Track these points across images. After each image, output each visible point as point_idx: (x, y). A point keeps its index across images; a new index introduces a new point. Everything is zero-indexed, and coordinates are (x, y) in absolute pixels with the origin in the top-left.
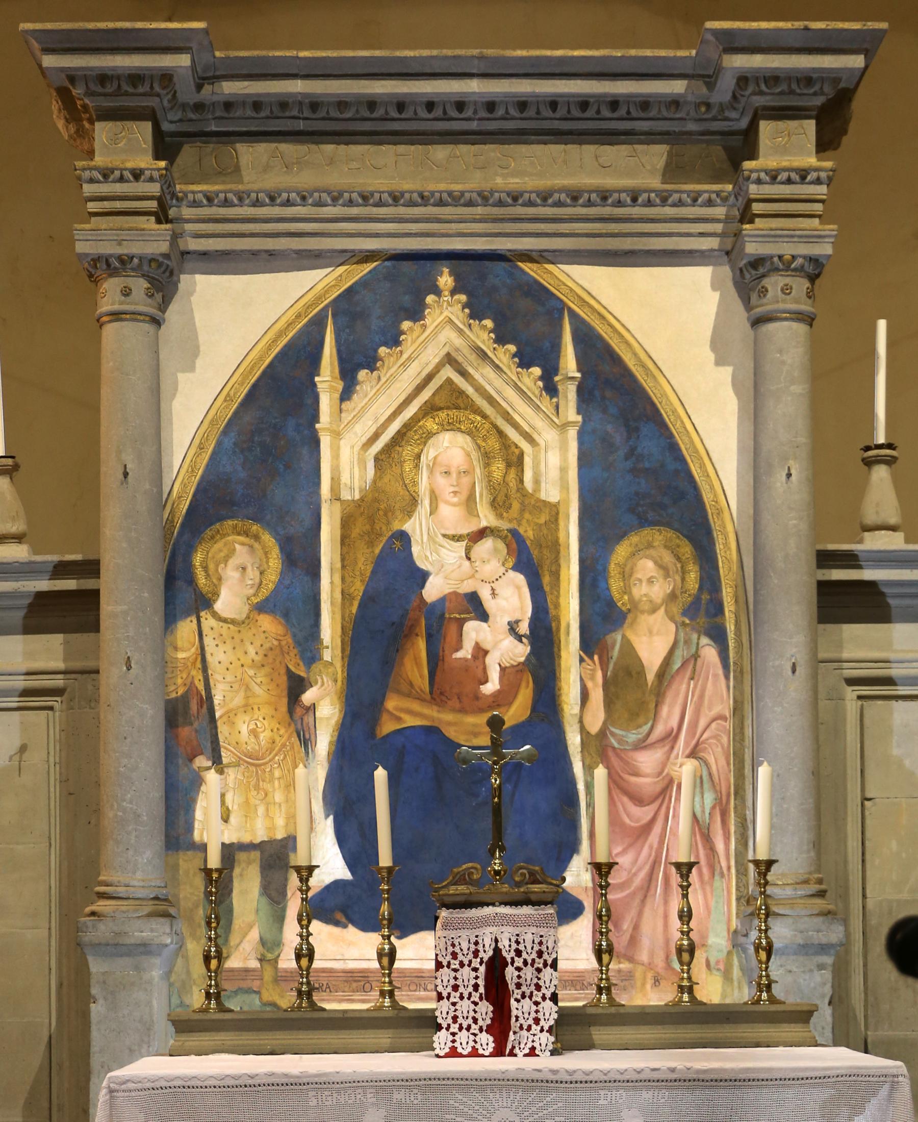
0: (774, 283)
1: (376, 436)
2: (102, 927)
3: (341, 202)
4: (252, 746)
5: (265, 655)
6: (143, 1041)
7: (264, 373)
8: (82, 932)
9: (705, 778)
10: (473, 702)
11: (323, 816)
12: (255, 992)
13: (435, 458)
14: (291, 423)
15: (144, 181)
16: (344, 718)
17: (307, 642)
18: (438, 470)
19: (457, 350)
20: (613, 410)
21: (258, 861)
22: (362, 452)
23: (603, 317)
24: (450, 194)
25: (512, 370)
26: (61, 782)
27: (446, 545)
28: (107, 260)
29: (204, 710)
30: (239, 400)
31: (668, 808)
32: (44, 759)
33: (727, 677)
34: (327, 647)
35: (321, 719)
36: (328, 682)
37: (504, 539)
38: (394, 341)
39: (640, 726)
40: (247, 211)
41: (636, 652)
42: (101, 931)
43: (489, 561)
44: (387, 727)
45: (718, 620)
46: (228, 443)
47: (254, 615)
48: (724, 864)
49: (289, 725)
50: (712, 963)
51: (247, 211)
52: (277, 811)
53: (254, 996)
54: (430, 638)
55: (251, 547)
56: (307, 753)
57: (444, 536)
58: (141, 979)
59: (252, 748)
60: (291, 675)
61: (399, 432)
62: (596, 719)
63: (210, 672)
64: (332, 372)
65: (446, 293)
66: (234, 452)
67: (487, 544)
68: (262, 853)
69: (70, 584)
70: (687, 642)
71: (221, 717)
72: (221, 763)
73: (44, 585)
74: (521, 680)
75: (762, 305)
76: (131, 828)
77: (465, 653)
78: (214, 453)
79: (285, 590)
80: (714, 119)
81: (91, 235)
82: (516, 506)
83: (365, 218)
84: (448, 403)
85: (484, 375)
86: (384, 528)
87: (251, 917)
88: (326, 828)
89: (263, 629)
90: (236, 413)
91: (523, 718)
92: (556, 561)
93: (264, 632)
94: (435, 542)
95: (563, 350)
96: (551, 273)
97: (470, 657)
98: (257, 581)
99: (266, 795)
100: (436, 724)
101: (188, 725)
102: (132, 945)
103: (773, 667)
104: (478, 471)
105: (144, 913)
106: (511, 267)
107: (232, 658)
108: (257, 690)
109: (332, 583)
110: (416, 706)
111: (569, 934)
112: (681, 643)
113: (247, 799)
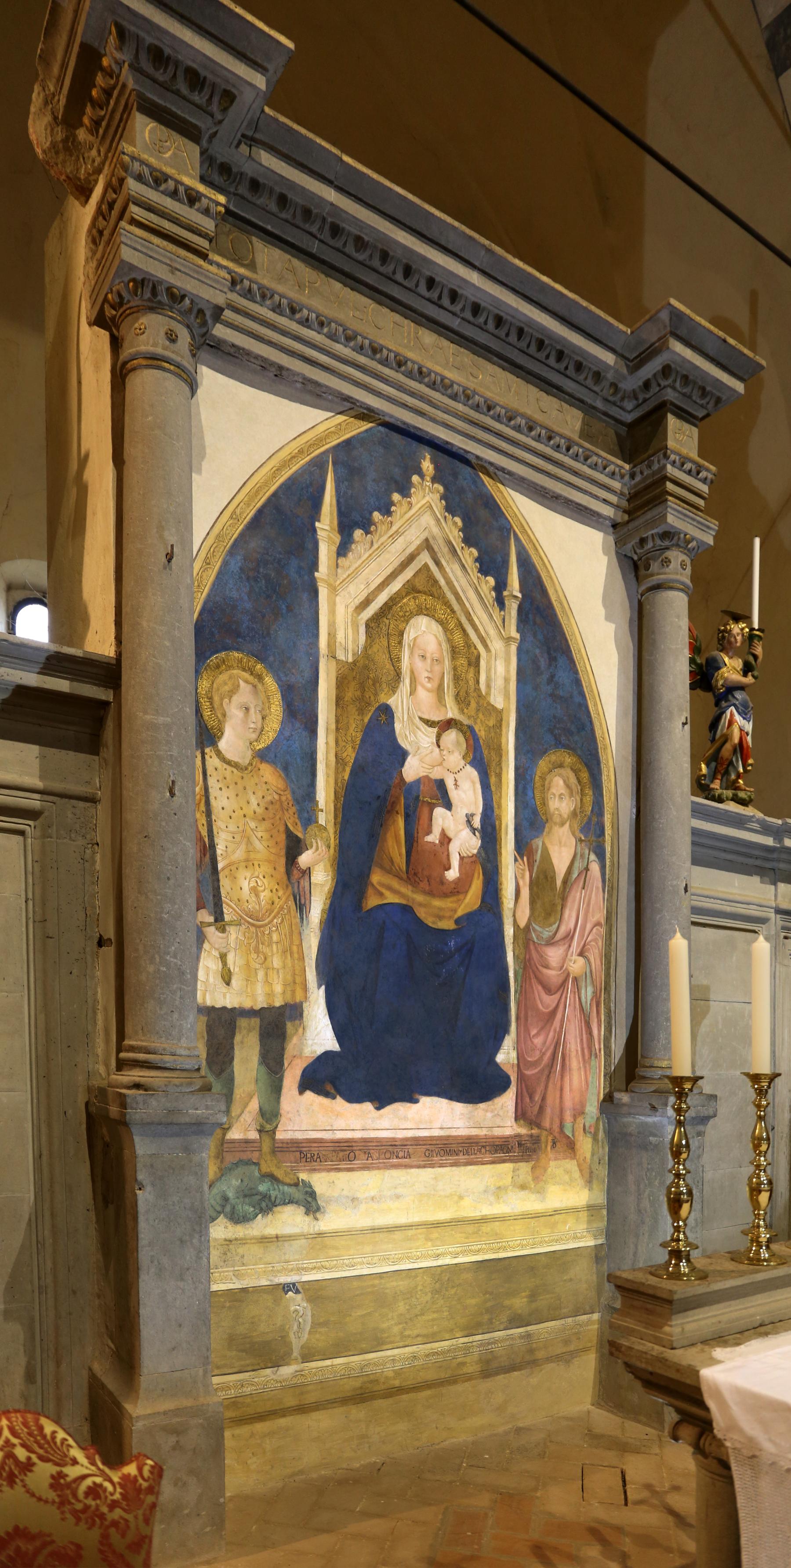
1: (366, 603)
2: (153, 1102)
3: (352, 344)
4: (252, 906)
5: (267, 809)
6: (194, 1230)
7: (269, 500)
8: (132, 1108)
9: (588, 974)
11: (316, 985)
12: (254, 1163)
13: (415, 639)
14: (294, 563)
15: (197, 210)
16: (336, 887)
18: (417, 652)
19: (434, 538)
20: (540, 637)
21: (258, 1029)
22: (355, 615)
23: (536, 549)
24: (443, 378)
25: (474, 574)
26: (34, 922)
27: (421, 727)
28: (154, 288)
29: (207, 859)
30: (245, 522)
31: (566, 998)
33: (604, 891)
34: (322, 811)
35: (316, 884)
36: (323, 848)
37: (464, 733)
38: (387, 511)
39: (551, 925)
40: (265, 312)
41: (551, 859)
43: (453, 752)
44: (372, 901)
45: (601, 839)
46: (235, 565)
47: (256, 761)
48: (597, 1047)
49: (287, 886)
50: (587, 1128)
51: (265, 312)
52: (275, 977)
53: (253, 1167)
54: (407, 817)
55: (255, 686)
56: (302, 918)
57: (421, 719)
58: (191, 1161)
59: (253, 908)
60: (290, 835)
61: (386, 604)
63: (214, 817)
64: (331, 522)
65: (428, 478)
66: (240, 578)
67: (451, 737)
68: (261, 1020)
69: (62, 685)
70: (582, 856)
71: (223, 869)
72: (223, 920)
73: (31, 679)
74: (474, 871)
75: (665, 574)
76: (175, 986)
77: (433, 838)
78: (220, 573)
79: (285, 742)
80: (614, 404)
81: (143, 245)
82: (473, 705)
83: (372, 372)
85: (453, 569)
86: (372, 698)
87: (252, 1087)
89: (264, 779)
90: (242, 535)
91: (476, 907)
92: (499, 764)
93: (266, 783)
94: (413, 723)
95: (510, 568)
96: (502, 493)
97: (437, 842)
98: (259, 726)
99: (265, 959)
100: (410, 904)
102: (186, 1124)
103: (672, 886)
104: (447, 662)
105: (197, 1087)
106: (419, 483)
107: (235, 806)
108: (258, 845)
109: (327, 743)
110: (395, 884)
111: (500, 1104)
112: (579, 856)
113: (248, 961)
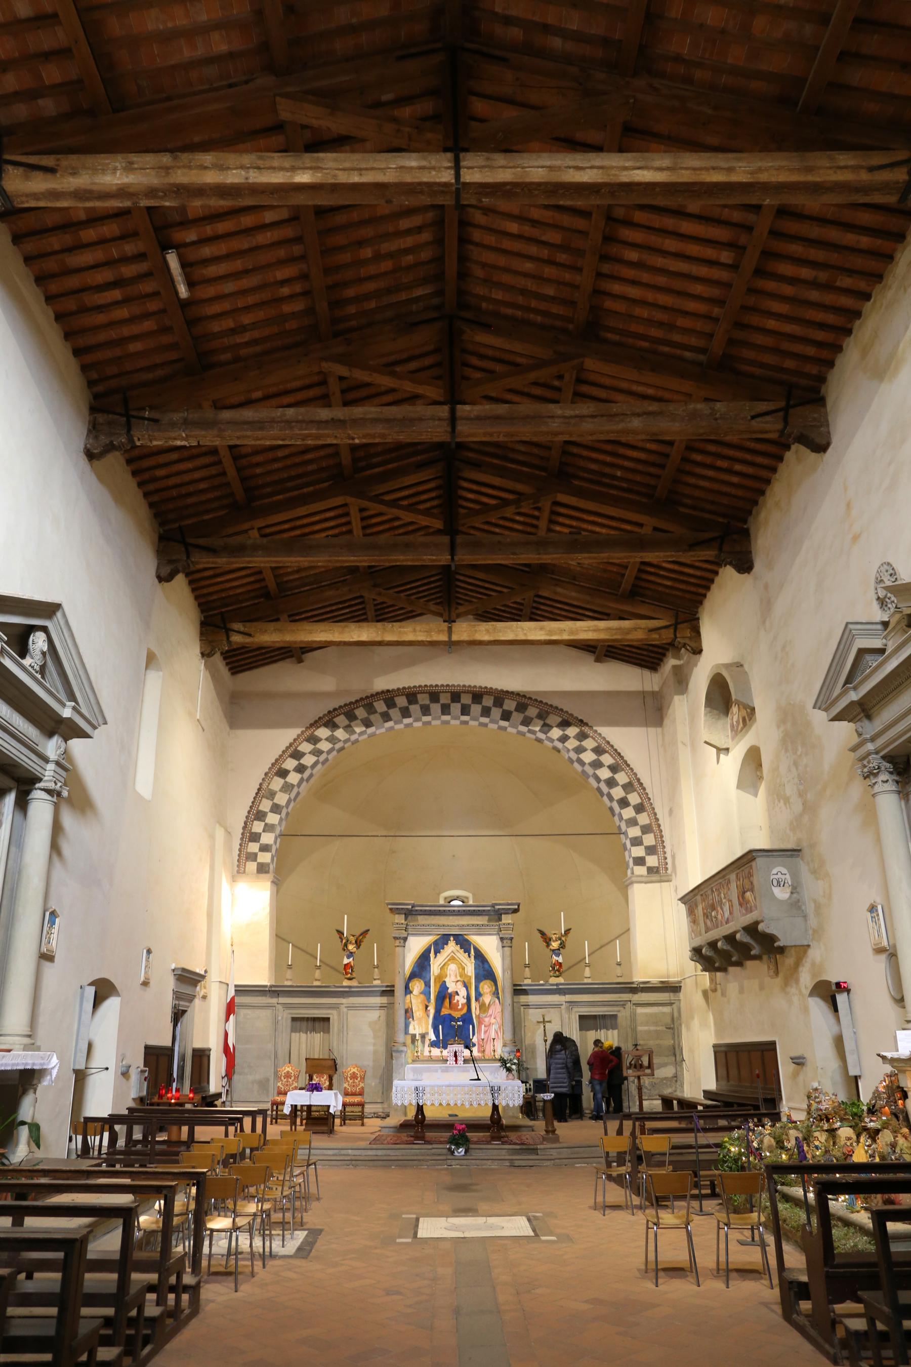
0: (505, 941)
8: (446, 431)
10: (457, 1010)
17: (429, 999)
32: (383, 1018)
42: (395, 1049)
62: (478, 1013)
84: (452, 959)
85: (458, 954)
88: (432, 1031)
101: (409, 1013)
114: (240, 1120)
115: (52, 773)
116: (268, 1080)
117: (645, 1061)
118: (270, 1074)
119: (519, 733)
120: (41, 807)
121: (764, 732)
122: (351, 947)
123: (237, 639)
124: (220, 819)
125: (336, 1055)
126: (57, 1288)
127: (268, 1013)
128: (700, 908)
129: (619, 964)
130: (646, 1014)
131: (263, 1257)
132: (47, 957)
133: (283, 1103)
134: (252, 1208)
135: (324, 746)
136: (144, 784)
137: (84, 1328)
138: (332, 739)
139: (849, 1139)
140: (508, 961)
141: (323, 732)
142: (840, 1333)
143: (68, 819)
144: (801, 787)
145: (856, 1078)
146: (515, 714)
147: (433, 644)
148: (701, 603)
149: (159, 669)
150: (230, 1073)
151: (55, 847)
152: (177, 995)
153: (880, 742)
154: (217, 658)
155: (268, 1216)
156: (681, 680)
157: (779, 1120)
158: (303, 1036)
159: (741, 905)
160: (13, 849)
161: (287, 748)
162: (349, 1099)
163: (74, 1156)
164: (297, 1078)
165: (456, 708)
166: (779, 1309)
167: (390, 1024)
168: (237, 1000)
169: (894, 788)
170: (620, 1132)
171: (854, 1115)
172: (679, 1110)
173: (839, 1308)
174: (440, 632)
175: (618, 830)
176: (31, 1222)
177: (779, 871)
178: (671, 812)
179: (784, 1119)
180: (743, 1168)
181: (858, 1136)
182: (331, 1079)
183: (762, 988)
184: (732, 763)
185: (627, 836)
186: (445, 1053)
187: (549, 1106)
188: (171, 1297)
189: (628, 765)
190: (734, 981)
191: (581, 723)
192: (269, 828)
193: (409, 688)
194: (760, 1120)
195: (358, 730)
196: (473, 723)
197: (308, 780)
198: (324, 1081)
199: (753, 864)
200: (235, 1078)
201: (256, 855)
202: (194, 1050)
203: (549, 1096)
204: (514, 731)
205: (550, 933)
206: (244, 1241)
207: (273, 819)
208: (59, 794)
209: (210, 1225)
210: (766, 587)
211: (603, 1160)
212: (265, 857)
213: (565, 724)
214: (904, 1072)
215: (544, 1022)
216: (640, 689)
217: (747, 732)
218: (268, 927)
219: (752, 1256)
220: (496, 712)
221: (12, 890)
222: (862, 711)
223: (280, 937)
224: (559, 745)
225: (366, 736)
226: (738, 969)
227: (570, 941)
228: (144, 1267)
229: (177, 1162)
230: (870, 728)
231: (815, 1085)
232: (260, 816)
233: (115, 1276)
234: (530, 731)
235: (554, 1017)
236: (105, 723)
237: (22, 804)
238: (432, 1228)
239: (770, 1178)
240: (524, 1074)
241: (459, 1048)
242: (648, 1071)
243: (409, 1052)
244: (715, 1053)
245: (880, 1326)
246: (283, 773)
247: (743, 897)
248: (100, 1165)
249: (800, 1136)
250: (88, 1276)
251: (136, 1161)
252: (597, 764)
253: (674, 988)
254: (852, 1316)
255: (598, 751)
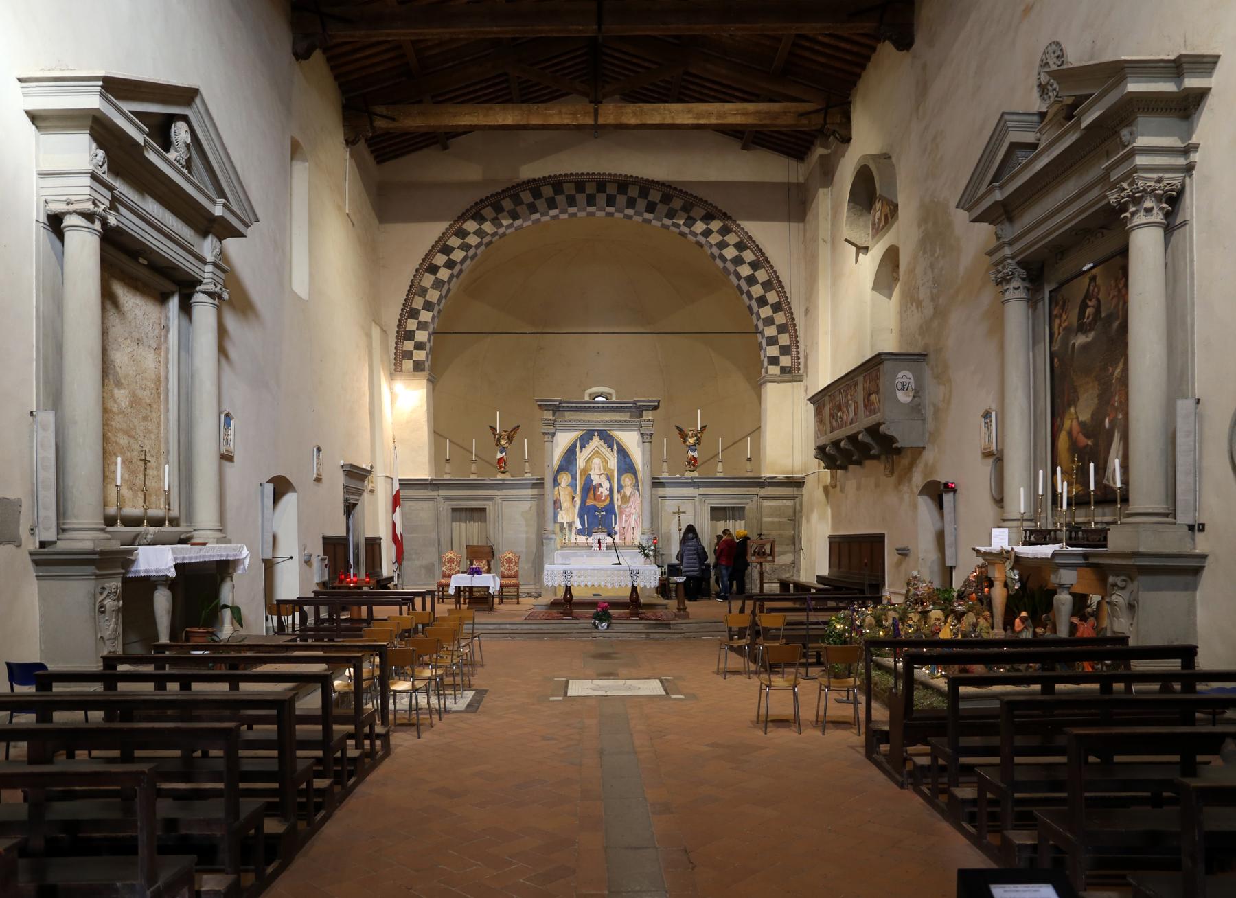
10: (600, 501)
32: (534, 508)
84: (597, 453)
101: (557, 503)
114: (412, 601)
115: (210, 275)
116: (433, 565)
117: (768, 549)
118: (435, 559)
119: (664, 226)
120: (204, 310)
121: (904, 233)
122: (503, 442)
123: (380, 123)
124: (376, 320)
125: (493, 542)
126: (274, 737)
127: (430, 504)
128: (827, 409)
129: (749, 460)
130: (771, 507)
131: (439, 712)
132: (227, 458)
133: (448, 585)
134: (427, 673)
135: (473, 240)
136: (300, 283)
137: (301, 766)
138: (480, 233)
139: (938, 619)
140: (647, 456)
141: (471, 226)
142: (909, 766)
143: (231, 322)
144: (935, 291)
145: (951, 569)
146: (660, 206)
147: (579, 127)
148: (854, 84)
149: (304, 160)
150: (399, 558)
151: (222, 350)
152: (348, 490)
153: (1018, 246)
154: (362, 145)
155: (441, 679)
156: (827, 173)
157: (880, 602)
158: (463, 525)
159: (865, 406)
160: (182, 353)
161: (437, 242)
162: (505, 581)
163: (271, 633)
164: (459, 563)
165: (601, 198)
166: (863, 751)
167: (541, 514)
168: (402, 493)
169: (1024, 296)
170: (742, 610)
171: (945, 600)
172: (795, 592)
173: (910, 749)
174: (586, 114)
175: (755, 332)
176: (245, 687)
177: (905, 375)
178: (807, 311)
179: (885, 602)
180: (845, 642)
181: (946, 617)
182: (489, 564)
183: (877, 486)
184: (868, 264)
185: (763, 336)
186: (590, 540)
187: (681, 587)
188: (367, 742)
189: (769, 262)
190: (852, 479)
191: (725, 216)
192: (422, 326)
193: (555, 176)
194: (864, 603)
195: (505, 223)
196: (618, 215)
197: (458, 276)
198: (483, 565)
199: (881, 367)
200: (404, 563)
201: (411, 353)
202: (367, 539)
203: (682, 579)
204: (658, 224)
205: (688, 430)
206: (422, 700)
207: (426, 316)
208: (220, 297)
209: (394, 688)
210: (924, 66)
211: (726, 634)
212: (420, 355)
213: (708, 218)
214: (993, 564)
215: (679, 513)
216: (786, 180)
217: (888, 230)
218: (425, 428)
219: (847, 711)
220: (641, 204)
221: (187, 394)
222: (1002, 213)
223: (438, 434)
224: (702, 239)
225: (512, 230)
226: (857, 467)
227: (705, 437)
228: (344, 720)
229: (361, 636)
230: (1010, 231)
231: (915, 573)
232: (414, 314)
233: (320, 727)
234: (674, 225)
235: (689, 509)
236: (257, 221)
237: (186, 308)
238: (578, 688)
239: (867, 650)
240: (659, 559)
241: (602, 535)
242: (770, 558)
243: (558, 540)
244: (830, 543)
245: (941, 762)
246: (433, 269)
247: (868, 399)
248: (295, 640)
249: (897, 616)
250: (298, 727)
251: (326, 636)
252: (738, 261)
253: (797, 483)
254: (920, 755)
255: (740, 246)
